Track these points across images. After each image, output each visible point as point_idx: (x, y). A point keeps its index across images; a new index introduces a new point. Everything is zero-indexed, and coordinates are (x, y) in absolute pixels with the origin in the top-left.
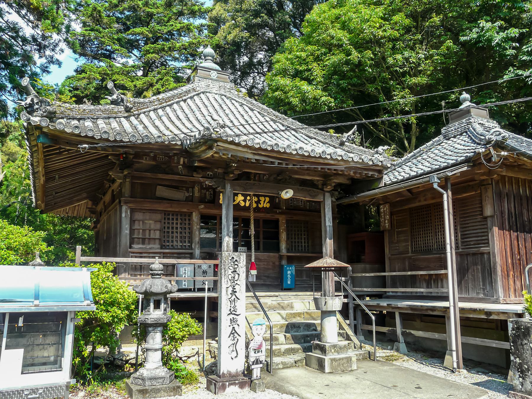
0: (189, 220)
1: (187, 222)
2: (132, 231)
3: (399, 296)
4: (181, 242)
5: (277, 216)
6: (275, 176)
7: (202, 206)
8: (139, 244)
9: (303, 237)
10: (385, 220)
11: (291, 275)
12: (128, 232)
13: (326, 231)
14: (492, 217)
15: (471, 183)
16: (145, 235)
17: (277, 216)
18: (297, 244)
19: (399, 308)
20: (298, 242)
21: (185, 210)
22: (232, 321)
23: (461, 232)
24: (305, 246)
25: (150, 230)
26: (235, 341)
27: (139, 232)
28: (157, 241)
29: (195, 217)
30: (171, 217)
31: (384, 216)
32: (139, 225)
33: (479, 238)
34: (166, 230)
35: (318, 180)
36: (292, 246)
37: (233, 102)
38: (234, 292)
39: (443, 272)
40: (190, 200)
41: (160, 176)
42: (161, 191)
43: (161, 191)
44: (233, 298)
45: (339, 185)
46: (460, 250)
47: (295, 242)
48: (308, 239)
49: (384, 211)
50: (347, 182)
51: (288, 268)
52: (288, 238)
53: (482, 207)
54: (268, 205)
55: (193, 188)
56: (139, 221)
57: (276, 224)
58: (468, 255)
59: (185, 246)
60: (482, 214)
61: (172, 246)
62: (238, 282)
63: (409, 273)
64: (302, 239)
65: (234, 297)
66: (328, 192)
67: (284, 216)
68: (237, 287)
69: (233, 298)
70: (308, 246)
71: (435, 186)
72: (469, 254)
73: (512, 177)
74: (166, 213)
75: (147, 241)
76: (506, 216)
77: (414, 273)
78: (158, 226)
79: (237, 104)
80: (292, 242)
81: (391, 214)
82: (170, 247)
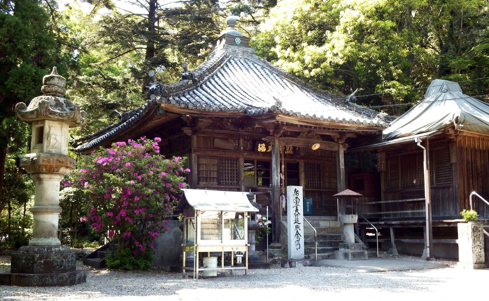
0: (236, 164)
1: (235, 165)
2: (199, 172)
3: (391, 219)
4: (231, 180)
5: (297, 160)
7: (246, 154)
8: (203, 181)
10: (381, 164)
11: (310, 205)
12: (196, 173)
13: (340, 172)
14: (455, 163)
15: (443, 141)
16: (207, 175)
17: (297, 160)
18: (312, 182)
19: (393, 225)
20: (313, 181)
21: (234, 156)
22: (297, 227)
24: (318, 183)
25: (210, 171)
26: (299, 239)
27: (203, 173)
28: (215, 180)
29: (242, 163)
30: (224, 161)
31: (381, 161)
32: (203, 168)
33: (447, 178)
35: (334, 136)
36: (308, 183)
37: (256, 65)
38: (297, 210)
40: (237, 149)
41: (216, 131)
42: (218, 143)
43: (218, 143)
44: (296, 214)
46: (435, 186)
47: (310, 181)
50: (355, 136)
51: (307, 200)
52: (305, 177)
54: (292, 153)
55: (239, 140)
56: (203, 164)
57: (297, 166)
58: (439, 188)
59: (234, 183)
60: (449, 161)
61: (225, 183)
62: (299, 204)
63: (400, 201)
64: (315, 178)
65: (297, 213)
66: (342, 144)
67: (302, 161)
68: (294, 204)
69: (296, 214)
71: (419, 144)
72: (440, 188)
73: (470, 137)
74: (220, 159)
76: (465, 163)
77: (404, 200)
78: (216, 169)
79: (259, 67)
80: (308, 180)
81: (387, 160)
82: (224, 184)
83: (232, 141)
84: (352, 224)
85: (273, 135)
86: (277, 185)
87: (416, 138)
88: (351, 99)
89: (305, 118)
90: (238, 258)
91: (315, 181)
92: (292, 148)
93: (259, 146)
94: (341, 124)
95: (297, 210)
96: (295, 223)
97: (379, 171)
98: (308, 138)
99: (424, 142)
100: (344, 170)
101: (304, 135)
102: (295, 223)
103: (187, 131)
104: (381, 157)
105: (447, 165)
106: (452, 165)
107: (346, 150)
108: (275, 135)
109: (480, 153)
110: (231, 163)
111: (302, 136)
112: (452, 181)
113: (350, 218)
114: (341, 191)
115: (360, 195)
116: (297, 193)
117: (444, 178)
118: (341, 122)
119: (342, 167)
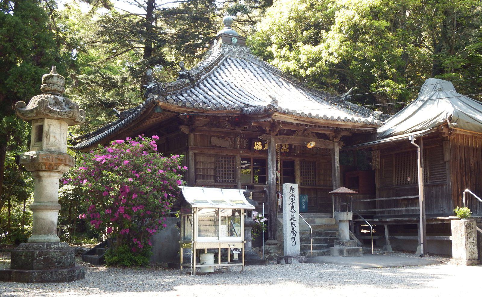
0: (233, 162)
2: (196, 169)
5: (293, 158)
6: (302, 131)
7: (243, 152)
8: (200, 179)
9: (312, 174)
11: (305, 202)
13: (335, 170)
14: (449, 161)
17: (293, 158)
18: (307, 179)
19: (387, 222)
21: (230, 154)
22: (292, 224)
23: (430, 171)
25: (207, 169)
26: (294, 236)
27: (200, 171)
28: (212, 177)
29: (238, 160)
30: (221, 159)
32: (200, 166)
34: (218, 169)
35: (330, 134)
37: (252, 64)
38: (293, 207)
39: (416, 196)
40: (234, 147)
42: (215, 141)
43: (215, 141)
44: (292, 211)
45: (344, 136)
46: (429, 183)
47: (306, 178)
48: (315, 175)
49: (375, 155)
51: (303, 197)
52: (301, 175)
53: (443, 154)
55: (235, 138)
56: (200, 162)
57: (292, 163)
59: (231, 181)
61: (222, 180)
62: (295, 201)
63: (394, 198)
65: (293, 210)
66: (337, 142)
67: (298, 158)
69: (292, 211)
70: (315, 181)
71: (413, 142)
73: (463, 135)
75: (206, 177)
76: (459, 161)
78: (213, 167)
79: (255, 66)
81: (381, 157)
83: (229, 139)
84: (347, 221)
85: (269, 134)
86: (273, 182)
87: (410, 136)
88: (346, 97)
89: (301, 117)
90: (235, 255)
91: (311, 179)
92: (287, 146)
93: (255, 144)
94: (337, 123)
95: (293, 207)
96: (290, 220)
97: (373, 169)
98: (304, 136)
99: (418, 140)
100: (339, 168)
101: (300, 133)
102: (290, 220)
103: (185, 129)
104: (376, 155)
105: (441, 163)
106: (445, 163)
107: (341, 148)
108: (272, 133)
109: (474, 151)
110: (228, 161)
111: (298, 134)
112: (446, 178)
113: (345, 215)
114: (336, 188)
115: (355, 192)
116: (292, 191)
117: (437, 176)
118: (336, 120)
119: (337, 164)
